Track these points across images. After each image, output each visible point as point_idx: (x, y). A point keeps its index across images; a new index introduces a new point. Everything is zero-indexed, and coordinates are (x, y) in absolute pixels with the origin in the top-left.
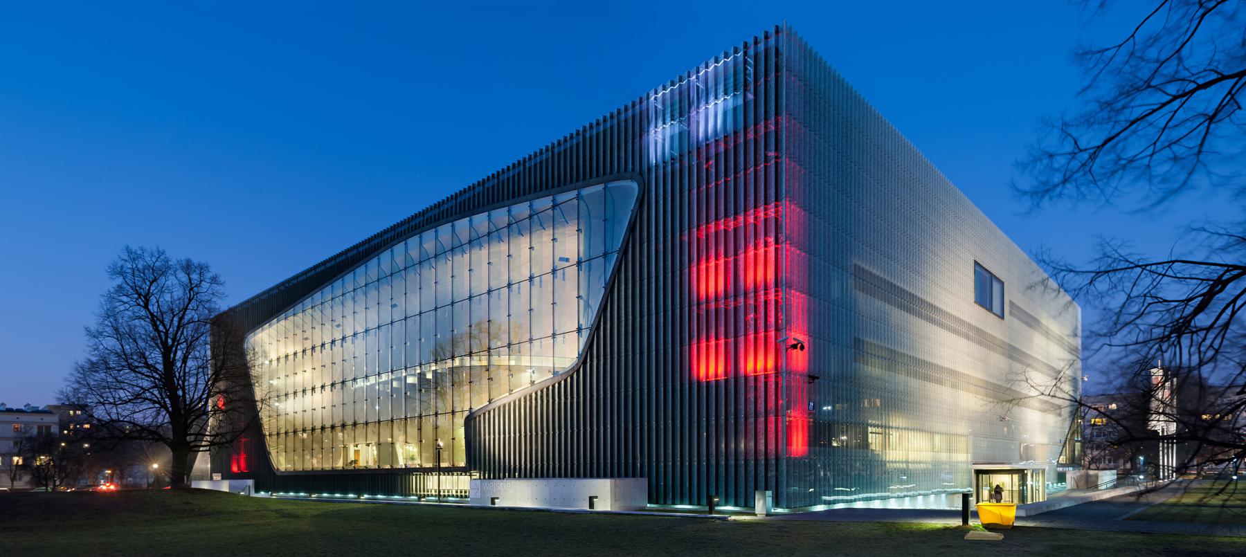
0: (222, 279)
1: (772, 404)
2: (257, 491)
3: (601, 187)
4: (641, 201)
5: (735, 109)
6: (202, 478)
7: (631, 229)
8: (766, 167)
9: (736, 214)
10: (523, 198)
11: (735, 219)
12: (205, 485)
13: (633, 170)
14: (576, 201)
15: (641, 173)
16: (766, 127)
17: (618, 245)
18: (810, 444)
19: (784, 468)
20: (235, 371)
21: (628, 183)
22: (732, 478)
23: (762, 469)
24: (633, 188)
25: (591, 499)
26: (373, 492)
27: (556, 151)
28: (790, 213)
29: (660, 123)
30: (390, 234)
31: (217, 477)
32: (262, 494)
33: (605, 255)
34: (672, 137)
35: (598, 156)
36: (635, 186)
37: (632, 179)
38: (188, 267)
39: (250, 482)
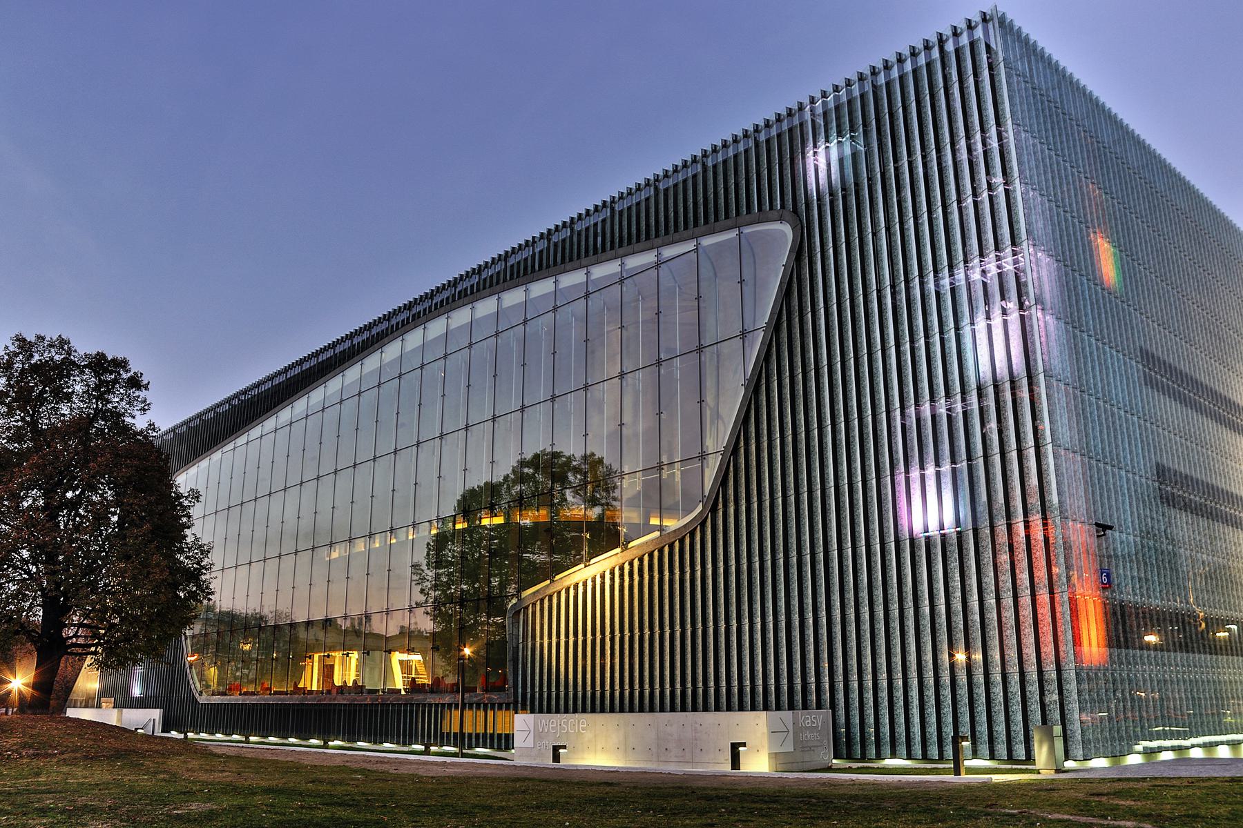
3: (733, 234)
4: (800, 252)
7: (786, 293)
8: (976, 204)
13: (783, 206)
14: (694, 255)
18: (1110, 646)
19: (1072, 687)
20: (164, 519)
22: (981, 708)
23: (1033, 689)
24: (785, 235)
25: (735, 747)
26: (351, 736)
27: (950, 47)
30: (445, 294)
31: (107, 703)
32: (174, 734)
33: (744, 334)
34: (841, 161)
35: (676, 212)
36: (785, 231)
37: (781, 219)
38: (100, 364)
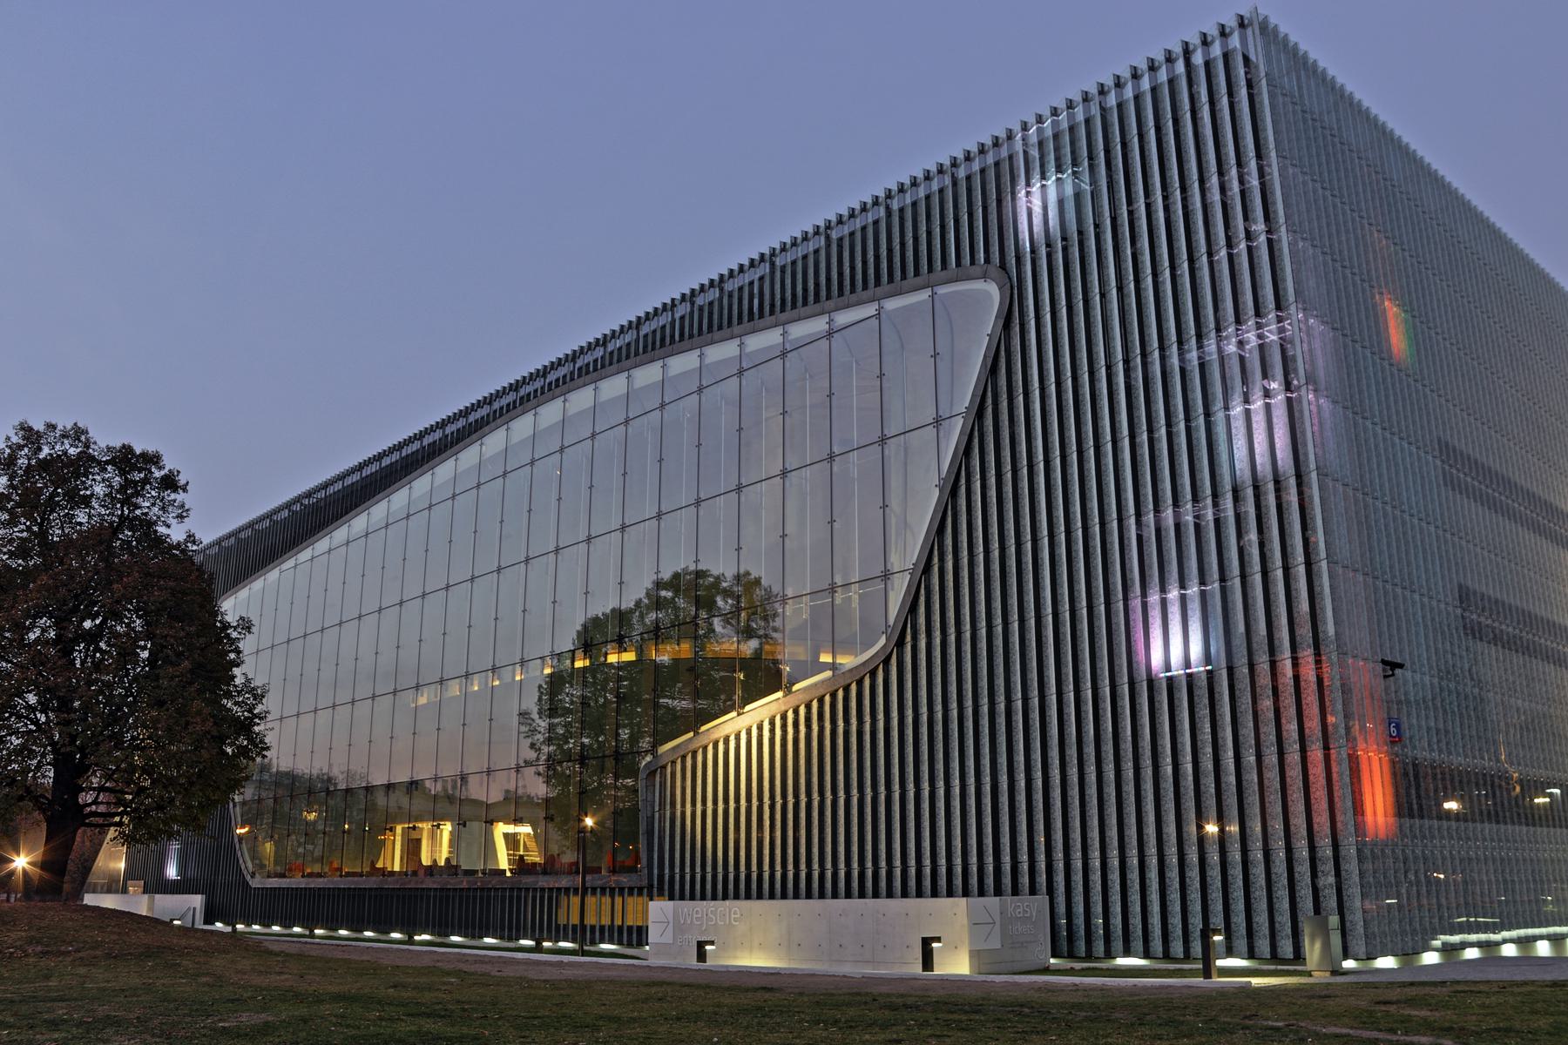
0: (182, 480)
1: (1313, 725)
2: (209, 920)
3: (924, 295)
5: (1078, 196)
6: (114, 885)
9: (1199, 336)
10: (726, 332)
11: (1200, 346)
12: (109, 902)
13: (987, 260)
15: (1003, 266)
16: (1241, 181)
17: (965, 397)
18: (1399, 813)
19: (1351, 867)
21: (979, 285)
24: (988, 295)
27: (1198, 59)
28: (1306, 331)
29: (1036, 176)
31: (134, 887)
35: (841, 274)
38: (125, 459)
39: (197, 901)
